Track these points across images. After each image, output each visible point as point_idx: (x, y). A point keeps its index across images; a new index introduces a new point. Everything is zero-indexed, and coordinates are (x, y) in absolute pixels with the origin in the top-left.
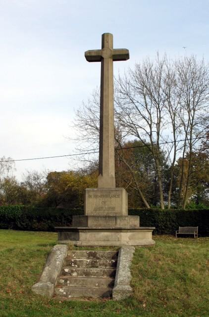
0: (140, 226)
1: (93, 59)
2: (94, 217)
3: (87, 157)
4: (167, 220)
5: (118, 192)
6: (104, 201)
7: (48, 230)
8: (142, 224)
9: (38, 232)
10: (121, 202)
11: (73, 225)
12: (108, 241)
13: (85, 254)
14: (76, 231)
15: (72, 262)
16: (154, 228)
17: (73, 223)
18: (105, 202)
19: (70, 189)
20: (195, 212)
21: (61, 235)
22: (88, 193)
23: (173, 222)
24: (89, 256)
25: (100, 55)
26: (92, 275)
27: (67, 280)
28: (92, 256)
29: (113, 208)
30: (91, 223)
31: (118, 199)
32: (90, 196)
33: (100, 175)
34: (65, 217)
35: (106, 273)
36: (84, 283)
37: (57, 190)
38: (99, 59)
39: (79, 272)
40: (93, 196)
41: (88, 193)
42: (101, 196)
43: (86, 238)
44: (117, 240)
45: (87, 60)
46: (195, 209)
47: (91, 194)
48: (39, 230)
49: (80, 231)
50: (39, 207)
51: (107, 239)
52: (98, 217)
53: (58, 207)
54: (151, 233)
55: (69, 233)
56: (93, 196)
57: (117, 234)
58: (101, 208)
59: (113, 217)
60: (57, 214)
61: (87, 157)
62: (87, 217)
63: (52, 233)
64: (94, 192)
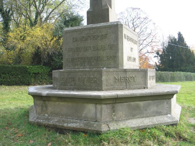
11: (104, 87)
17: (104, 83)
55: (141, 103)
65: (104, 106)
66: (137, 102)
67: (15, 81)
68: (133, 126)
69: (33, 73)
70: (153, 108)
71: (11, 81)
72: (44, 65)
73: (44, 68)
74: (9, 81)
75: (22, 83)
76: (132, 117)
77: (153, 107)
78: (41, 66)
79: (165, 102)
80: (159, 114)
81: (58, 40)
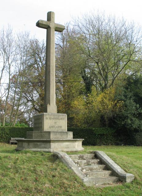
0: (73, 138)
1: (43, 26)
2: (54, 132)
4: (2, 133)
5: (63, 116)
10: (63, 122)
11: (34, 137)
12: (68, 148)
13: (77, 157)
16: (84, 139)
17: (34, 136)
20: (19, 128)
22: (46, 116)
23: (7, 134)
24: (79, 158)
25: (48, 25)
26: (94, 170)
27: (88, 174)
28: (81, 158)
29: (61, 127)
32: (47, 118)
35: (101, 167)
36: (97, 175)
38: (47, 27)
39: (87, 169)
41: (46, 116)
42: (53, 119)
43: (55, 147)
44: (73, 147)
45: (37, 23)
46: (20, 127)
51: (67, 147)
52: (57, 132)
54: (81, 143)
55: (38, 143)
57: (73, 143)
58: (53, 127)
65: (26, 143)
66: (37, 143)
69: (99, 134)
70: (43, 145)
72: (109, 127)
73: (109, 130)
78: (106, 128)
79: (48, 144)
80: (46, 148)
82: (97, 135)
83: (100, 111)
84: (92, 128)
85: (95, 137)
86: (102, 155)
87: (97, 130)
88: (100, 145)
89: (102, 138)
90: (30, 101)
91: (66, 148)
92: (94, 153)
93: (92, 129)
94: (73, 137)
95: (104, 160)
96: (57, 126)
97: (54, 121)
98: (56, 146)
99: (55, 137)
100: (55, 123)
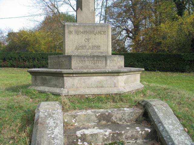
0: (125, 66)
3: (36, 18)
6: (87, 38)
7: (11, 67)
8: (127, 64)
9: (4, 68)
12: (102, 87)
14: (60, 75)
15: (77, 138)
18: (88, 40)
19: (24, 40)
21: (36, 80)
22: (68, 28)
29: (98, 47)
30: (76, 65)
31: (104, 37)
32: (70, 32)
33: (79, 9)
34: (21, 58)
37: (16, 40)
40: (74, 32)
41: (68, 28)
42: (85, 32)
43: (73, 85)
47: (72, 29)
48: (4, 67)
49: (64, 75)
50: (3, 52)
52: (84, 57)
53: (16, 52)
55: (47, 77)
56: (74, 32)
57: (113, 78)
58: (83, 47)
59: (103, 56)
60: (16, 56)
61: (36, 18)
62: (70, 57)
63: (13, 68)
64: (76, 28)
67: (170, 68)
68: (40, 90)
69: (188, 60)
71: (166, 67)
74: (164, 68)
75: (176, 70)
76: (43, 85)
77: (54, 81)
79: (61, 79)
81: (121, 31)
82: (186, 61)
83: (190, 34)
84: (181, 53)
85: (184, 64)
86: (160, 115)
87: (186, 55)
88: (189, 72)
89: (192, 64)
90: (125, 29)
91: (97, 87)
92: (144, 106)
93: (181, 54)
94: (124, 65)
95: (164, 134)
96: (90, 45)
97: (85, 36)
98: (75, 84)
99: (81, 65)
100: (88, 40)
